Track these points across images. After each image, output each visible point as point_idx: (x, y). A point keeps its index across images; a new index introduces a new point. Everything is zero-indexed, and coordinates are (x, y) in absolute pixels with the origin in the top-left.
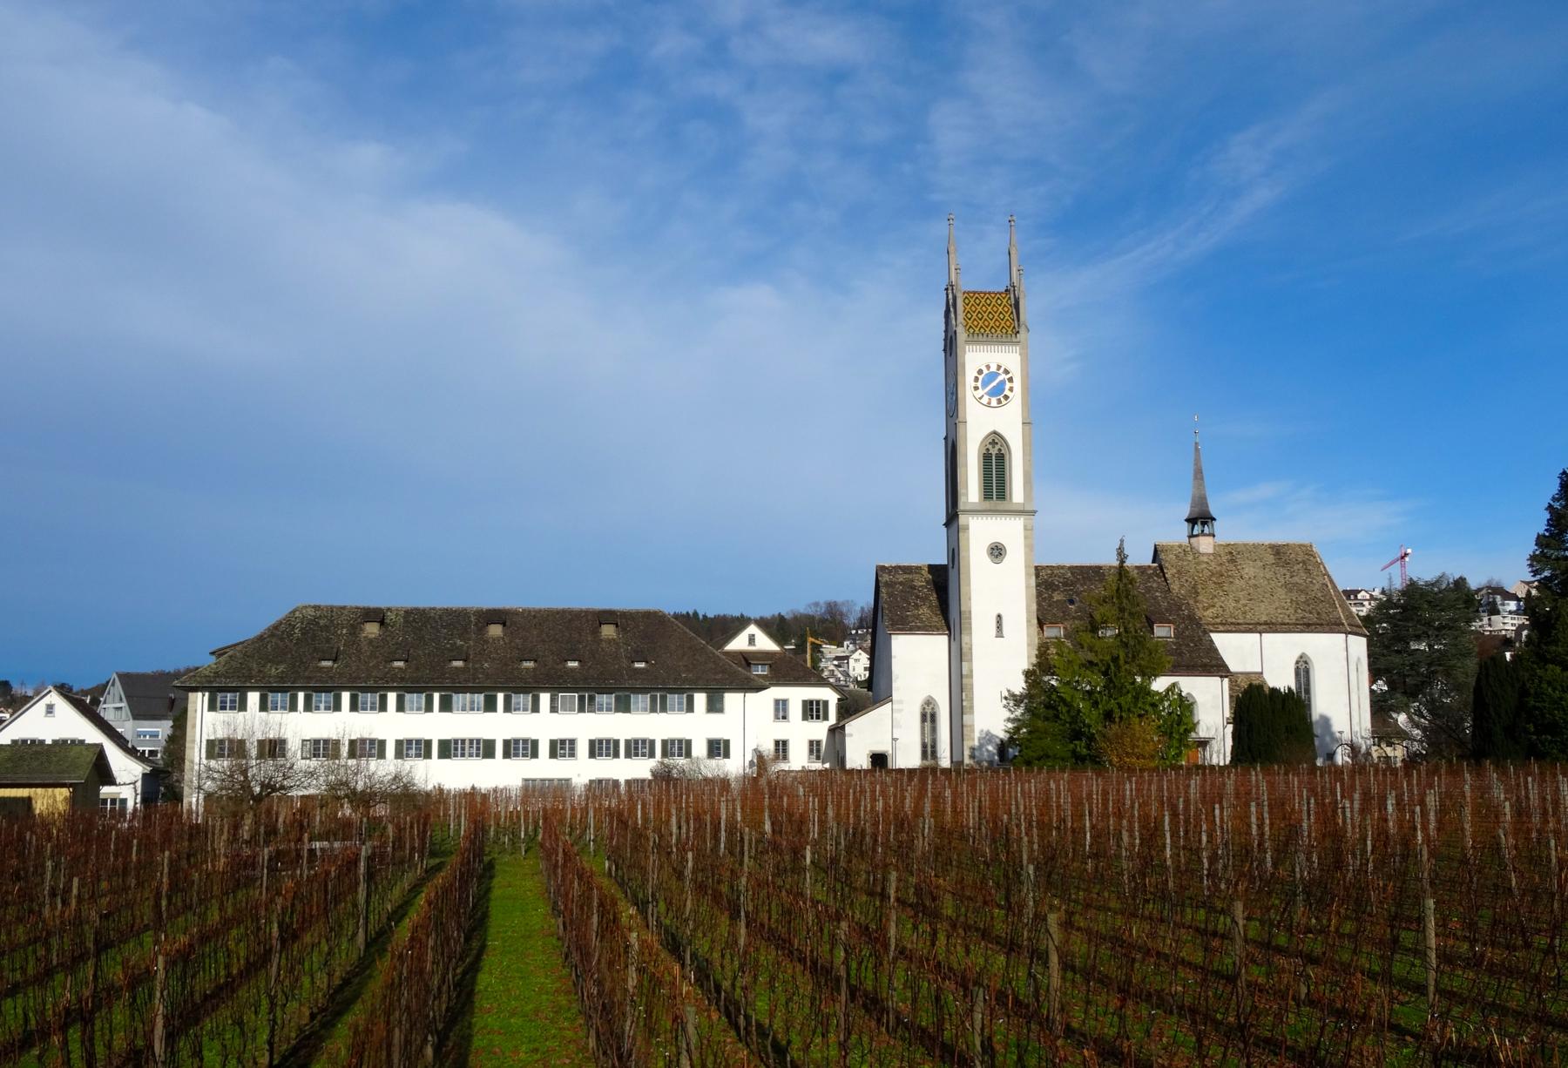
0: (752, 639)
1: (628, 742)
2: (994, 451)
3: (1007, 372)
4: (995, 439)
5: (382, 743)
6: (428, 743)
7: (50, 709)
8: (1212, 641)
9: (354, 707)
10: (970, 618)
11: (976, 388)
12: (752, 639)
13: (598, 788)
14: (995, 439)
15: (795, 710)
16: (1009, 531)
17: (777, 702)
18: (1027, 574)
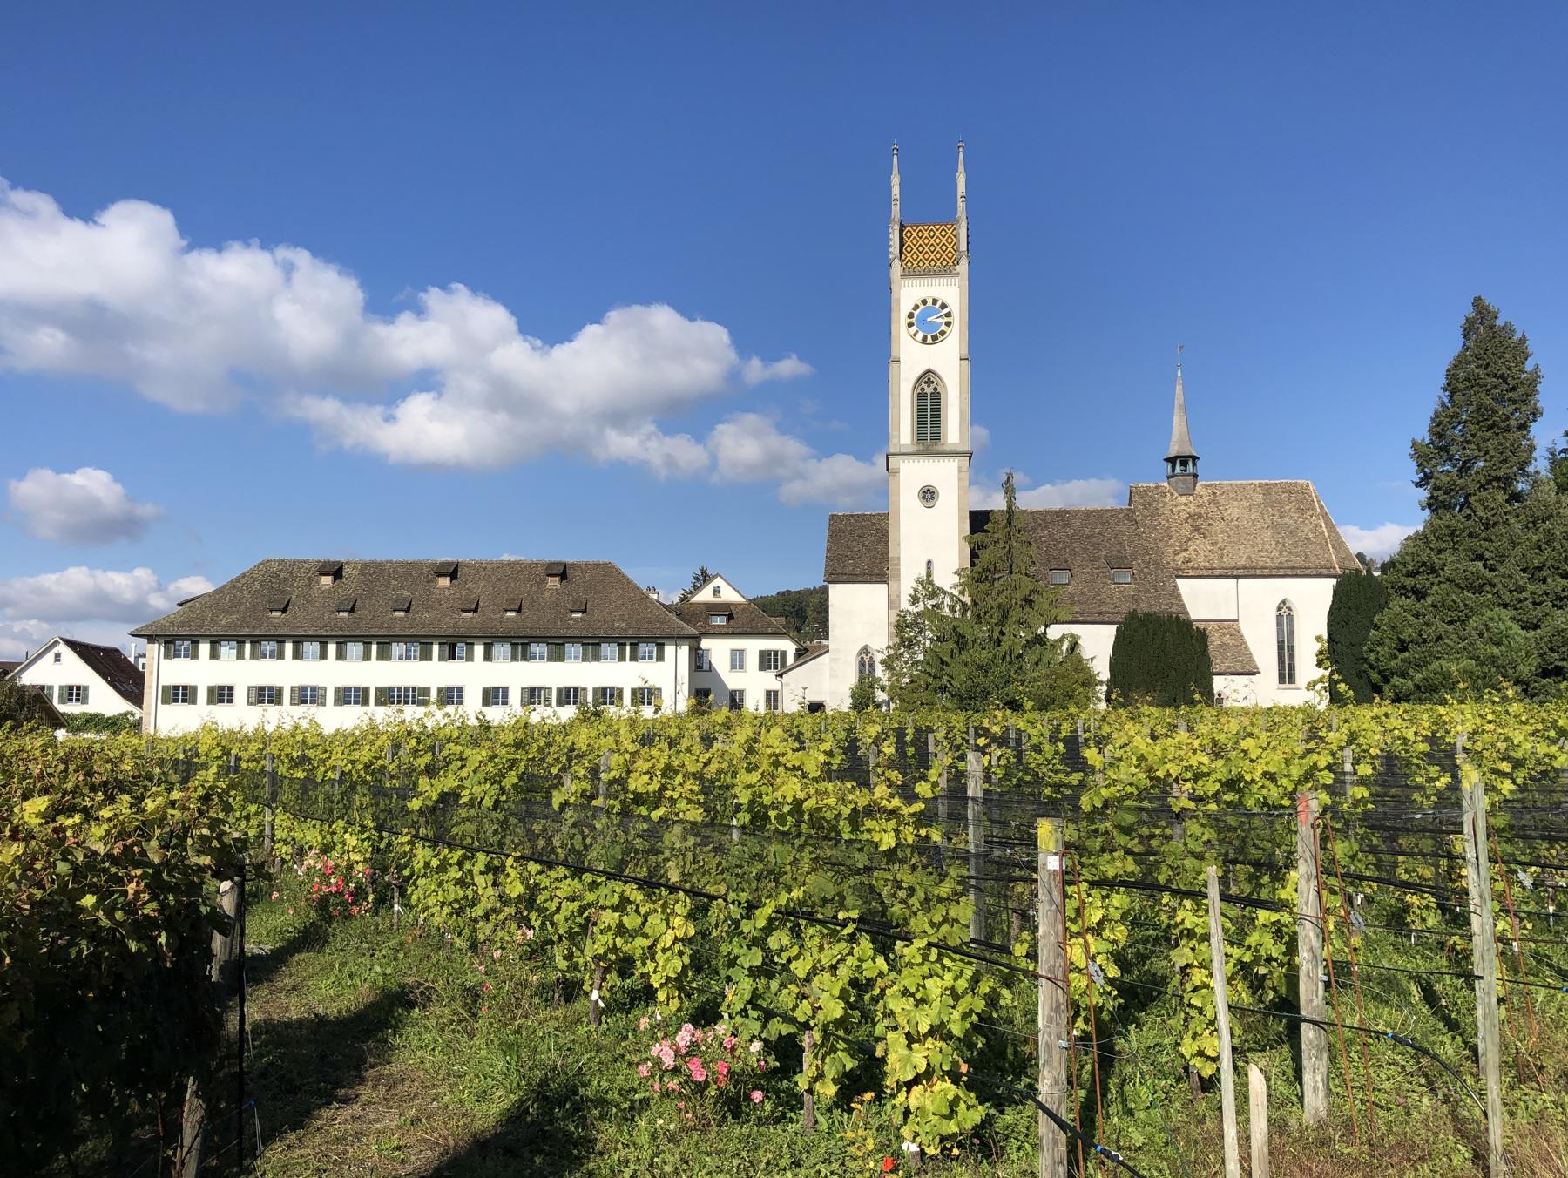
0: (717, 591)
1: (559, 691)
2: (929, 391)
3: (944, 306)
4: (928, 377)
5: (280, 691)
6: (366, 690)
7: (58, 657)
8: (1176, 586)
9: (488, 657)
10: (899, 565)
11: (910, 325)
12: (717, 591)
13: (352, 741)
14: (928, 377)
15: (752, 660)
16: (944, 474)
17: (733, 651)
18: (960, 518)
